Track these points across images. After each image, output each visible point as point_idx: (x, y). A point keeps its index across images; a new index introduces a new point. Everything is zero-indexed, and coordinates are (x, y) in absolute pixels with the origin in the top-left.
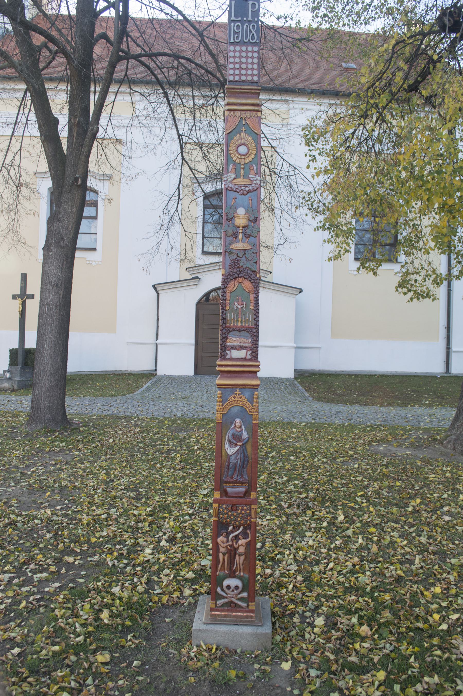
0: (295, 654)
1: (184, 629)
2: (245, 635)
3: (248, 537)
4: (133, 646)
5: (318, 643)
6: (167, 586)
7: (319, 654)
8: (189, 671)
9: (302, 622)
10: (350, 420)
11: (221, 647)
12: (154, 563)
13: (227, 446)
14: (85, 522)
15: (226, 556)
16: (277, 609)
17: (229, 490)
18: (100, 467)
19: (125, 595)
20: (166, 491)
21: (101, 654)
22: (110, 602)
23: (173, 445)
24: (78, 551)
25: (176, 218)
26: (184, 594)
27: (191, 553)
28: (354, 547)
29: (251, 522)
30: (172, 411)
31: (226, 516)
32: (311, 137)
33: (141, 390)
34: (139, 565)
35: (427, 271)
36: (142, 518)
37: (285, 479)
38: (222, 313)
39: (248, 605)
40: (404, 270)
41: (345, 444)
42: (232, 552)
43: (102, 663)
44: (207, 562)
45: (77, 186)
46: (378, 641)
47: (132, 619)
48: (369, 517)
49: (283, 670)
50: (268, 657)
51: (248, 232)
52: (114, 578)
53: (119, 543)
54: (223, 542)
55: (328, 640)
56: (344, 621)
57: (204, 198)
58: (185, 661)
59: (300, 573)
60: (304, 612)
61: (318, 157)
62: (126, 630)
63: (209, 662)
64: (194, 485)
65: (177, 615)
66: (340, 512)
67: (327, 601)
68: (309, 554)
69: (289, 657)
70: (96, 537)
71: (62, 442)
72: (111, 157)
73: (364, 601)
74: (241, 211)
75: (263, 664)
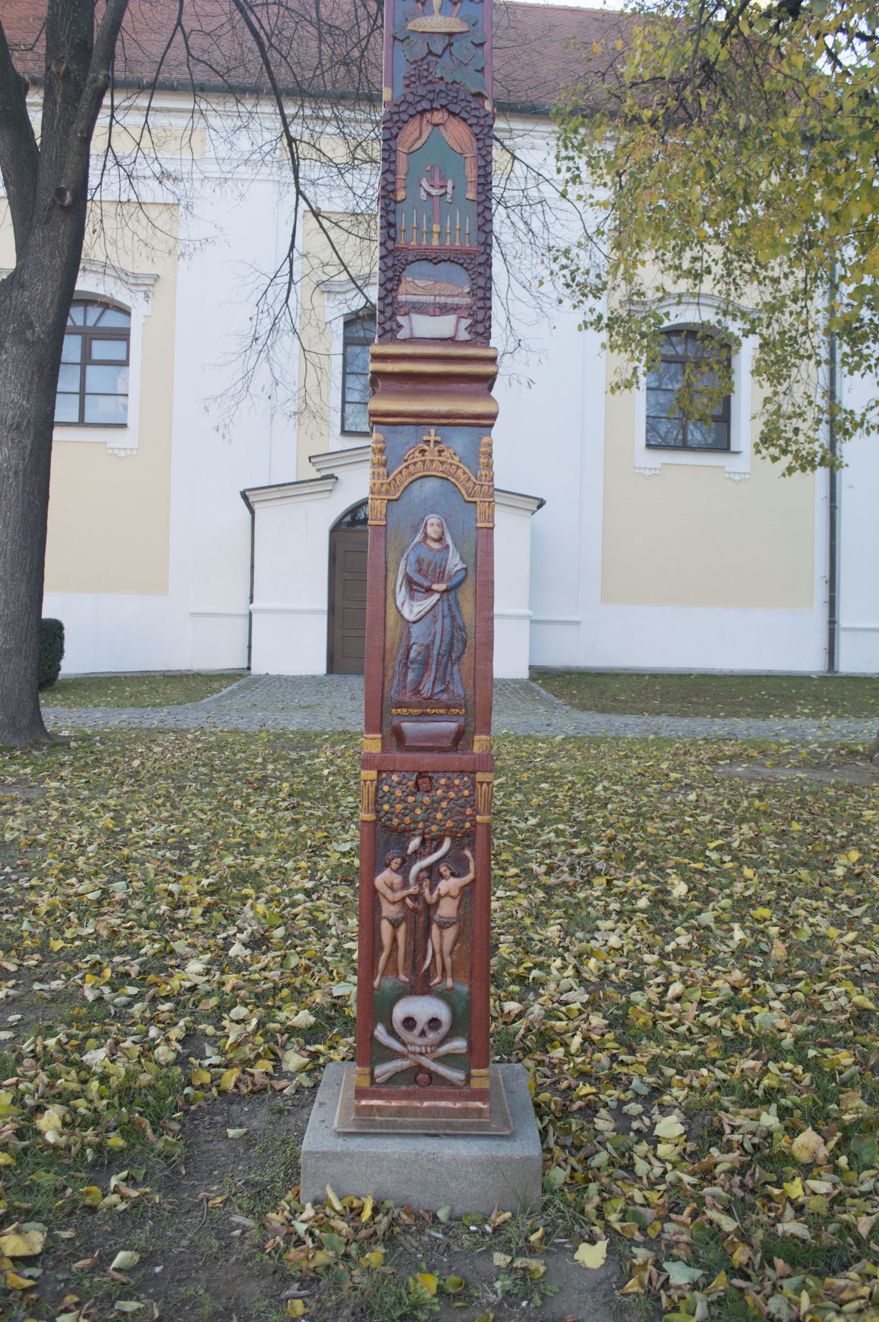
0: (613, 1218)
1: (280, 1158)
2: (457, 1167)
3: (467, 871)
4: (122, 1207)
5: (677, 1185)
6: (237, 1045)
7: (685, 1217)
8: (287, 1280)
9: (623, 1129)
11: (389, 1204)
12: (209, 994)
13: (401, 595)
14: (43, 908)
15: (402, 928)
16: (545, 1096)
17: (408, 727)
18: (103, 806)
19: (120, 1069)
20: (252, 847)
21: (18, 1231)
22: (75, 1086)
23: (274, 770)
24: (12, 968)
25: (284, 324)
26: (285, 1067)
27: (307, 969)
28: (724, 948)
29: (475, 824)
31: (399, 807)
33: (216, 696)
34: (167, 998)
36: (188, 899)
37: (533, 821)
39: (469, 1078)
40: (771, 407)
42: (420, 917)
43: (14, 1259)
44: (347, 989)
45: (62, 207)
46: (852, 1175)
47: (129, 1130)
48: (747, 888)
49: (582, 1268)
50: (534, 1231)
52: (95, 1029)
53: (122, 951)
54: (391, 888)
55: (707, 1176)
56: (740, 1122)
58: (276, 1249)
59: (598, 1009)
60: (621, 1103)
62: (106, 1162)
63: (353, 1249)
64: (319, 834)
65: (260, 1120)
66: (674, 879)
67: (679, 1072)
68: (612, 966)
69: (597, 1230)
70: (65, 940)
71: (25, 766)
73: (782, 1070)
75: (520, 1253)
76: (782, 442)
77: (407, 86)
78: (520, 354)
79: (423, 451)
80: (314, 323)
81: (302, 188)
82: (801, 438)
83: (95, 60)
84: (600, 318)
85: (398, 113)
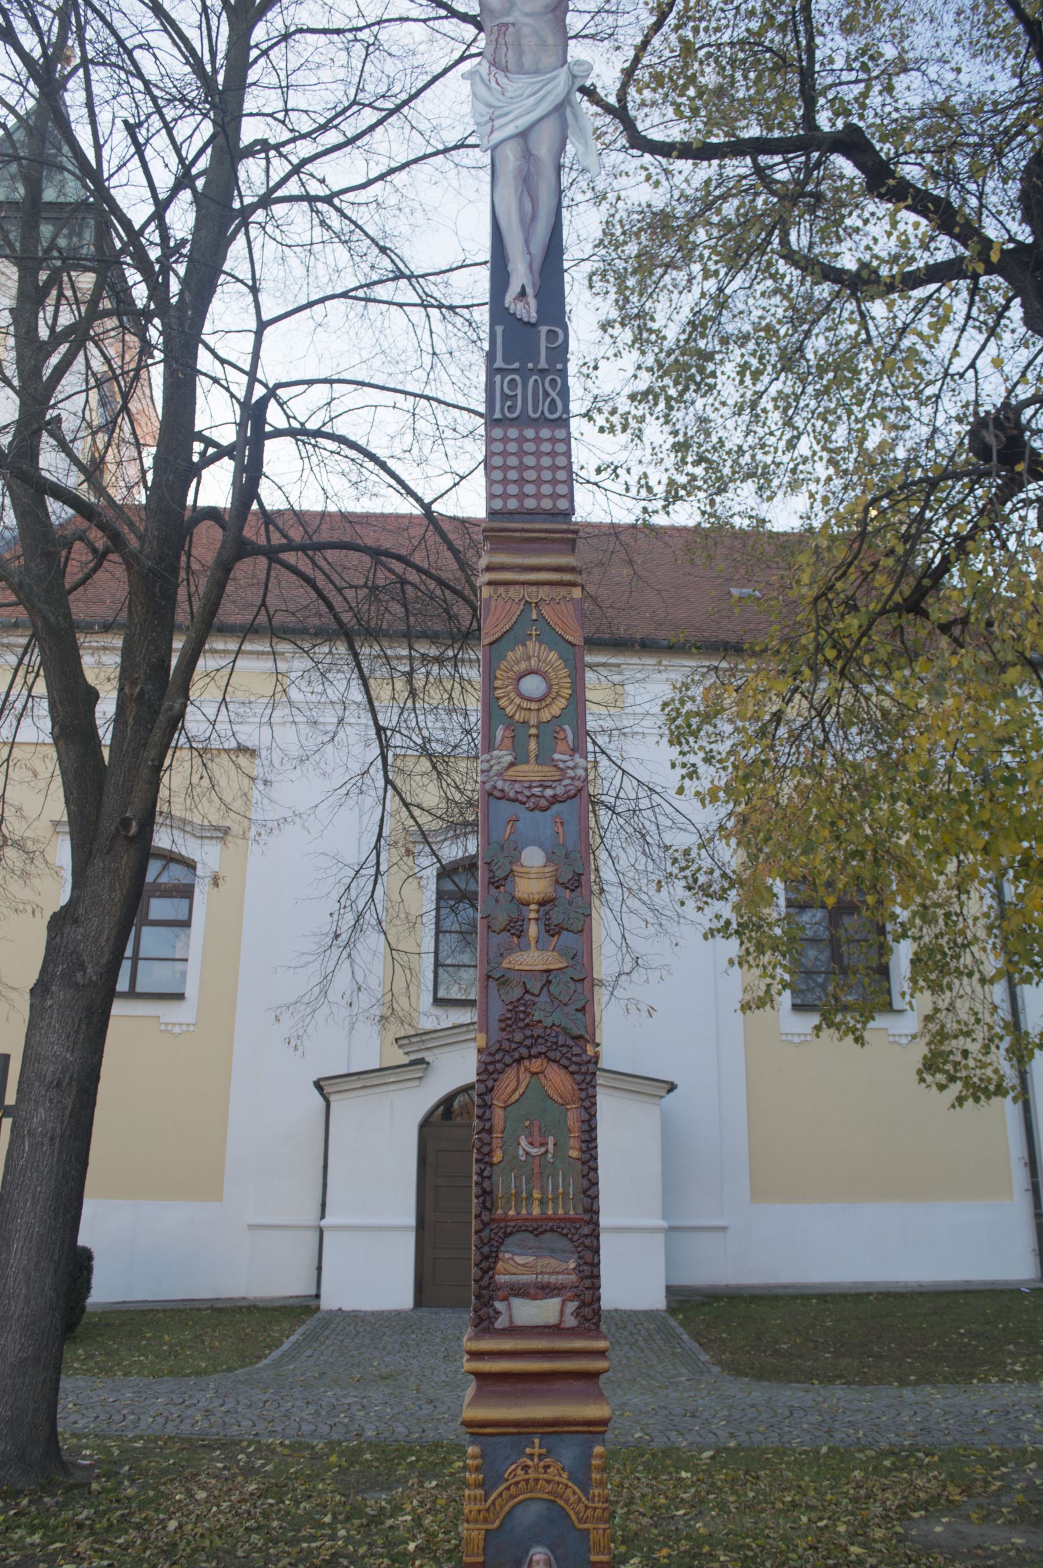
10: (830, 1432)
23: (348, 1539)
25: (370, 918)
30: (352, 1419)
32: (681, 731)
33: (276, 1354)
35: (991, 1028)
38: (480, 1174)
40: (934, 1027)
41: (834, 1519)
45: (126, 837)
51: (557, 916)
57: (439, 877)
61: (703, 768)
72: (222, 780)
74: (533, 857)
76: (948, 1067)
77: (503, 1030)
78: (639, 975)
79: (526, 1468)
80: (403, 916)
81: (391, 776)
82: (971, 1063)
83: (171, 690)
84: (728, 923)
85: (492, 1063)
